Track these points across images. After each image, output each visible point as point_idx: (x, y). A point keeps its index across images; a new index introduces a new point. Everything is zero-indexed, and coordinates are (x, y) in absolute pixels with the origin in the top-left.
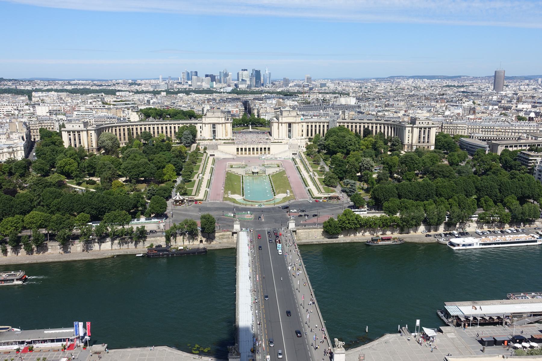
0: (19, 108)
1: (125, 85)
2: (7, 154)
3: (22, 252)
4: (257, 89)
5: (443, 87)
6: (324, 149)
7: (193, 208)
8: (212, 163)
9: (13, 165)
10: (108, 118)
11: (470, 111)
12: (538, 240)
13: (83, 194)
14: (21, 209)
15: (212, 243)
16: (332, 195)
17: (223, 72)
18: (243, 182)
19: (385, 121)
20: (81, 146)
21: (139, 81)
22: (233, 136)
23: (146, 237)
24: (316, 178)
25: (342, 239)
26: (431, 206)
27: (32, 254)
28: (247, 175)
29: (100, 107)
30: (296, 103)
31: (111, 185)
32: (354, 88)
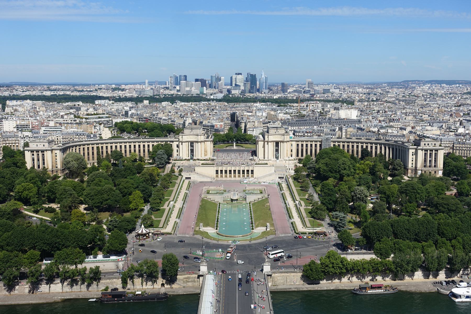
1: (108, 90)
4: (252, 95)
5: (464, 94)
7: (158, 244)
8: (187, 188)
10: (77, 134)
13: (37, 227)
16: (318, 230)
18: (219, 212)
19: (386, 140)
20: (45, 167)
21: (122, 86)
22: (213, 156)
23: (100, 279)
24: (302, 209)
25: (325, 285)
26: (430, 249)
28: (225, 202)
29: (71, 121)
30: (288, 117)
32: (361, 95)
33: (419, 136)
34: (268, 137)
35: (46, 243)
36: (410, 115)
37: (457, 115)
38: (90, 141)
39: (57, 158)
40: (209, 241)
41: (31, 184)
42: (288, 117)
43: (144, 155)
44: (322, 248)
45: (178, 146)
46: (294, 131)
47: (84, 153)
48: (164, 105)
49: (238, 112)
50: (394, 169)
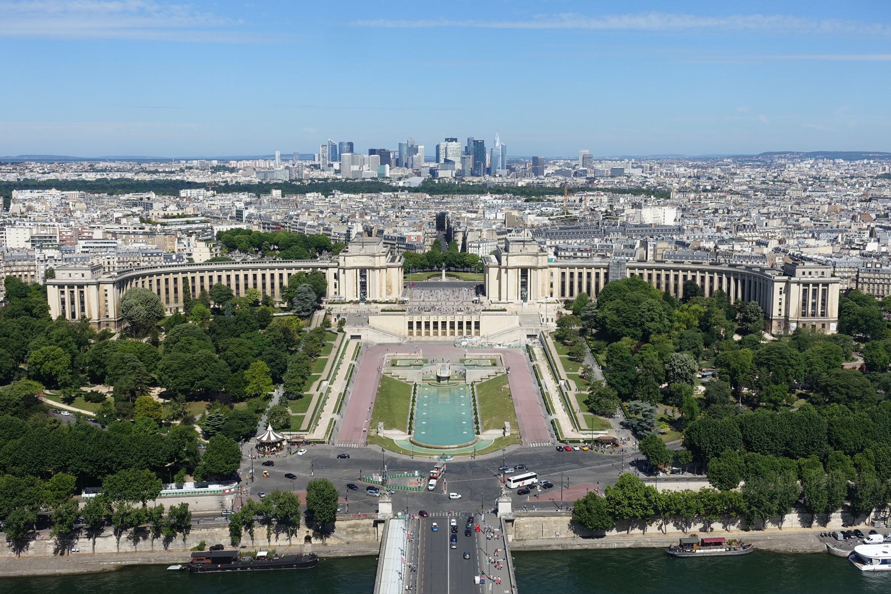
1: (204, 170)
4: (476, 179)
5: (878, 177)
7: (299, 461)
8: (354, 356)
10: (146, 254)
13: (71, 429)
16: (602, 434)
18: (414, 401)
19: (730, 266)
20: (84, 317)
21: (231, 162)
22: (404, 295)
23: (188, 528)
24: (572, 395)
25: (614, 538)
28: (426, 383)
29: (135, 228)
30: (546, 220)
31: (134, 406)
32: (683, 180)
33: (792, 256)
34: (507, 260)
35: (87, 460)
36: (775, 217)
37: (865, 217)
38: (170, 266)
39: (108, 298)
40: (395, 455)
41: (59, 349)
42: (546, 220)
43: (273, 293)
44: (609, 469)
45: (336, 277)
46: (557, 248)
47: (159, 290)
48: (311, 199)
49: (450, 213)
50: (746, 320)
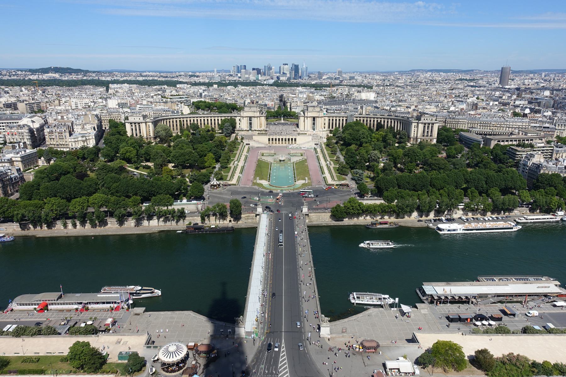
0: (94, 101)
2: (81, 142)
3: (88, 226)
4: (295, 81)
6: (342, 141)
7: (226, 192)
9: (85, 151)
10: (164, 111)
11: (473, 106)
12: (514, 227)
13: (138, 179)
14: (88, 191)
15: (238, 222)
17: (268, 66)
18: (270, 169)
19: (395, 116)
20: (141, 135)
21: (197, 73)
22: (267, 128)
23: (185, 217)
25: (347, 222)
27: (96, 228)
28: (275, 162)
30: (323, 98)
32: (378, 81)
33: (420, 113)
37: (450, 96)
42: (323, 98)
43: (215, 126)
47: (394, 126)
